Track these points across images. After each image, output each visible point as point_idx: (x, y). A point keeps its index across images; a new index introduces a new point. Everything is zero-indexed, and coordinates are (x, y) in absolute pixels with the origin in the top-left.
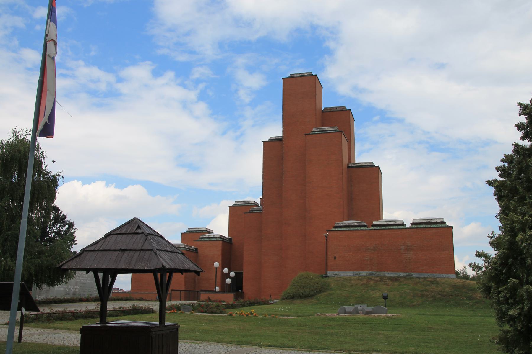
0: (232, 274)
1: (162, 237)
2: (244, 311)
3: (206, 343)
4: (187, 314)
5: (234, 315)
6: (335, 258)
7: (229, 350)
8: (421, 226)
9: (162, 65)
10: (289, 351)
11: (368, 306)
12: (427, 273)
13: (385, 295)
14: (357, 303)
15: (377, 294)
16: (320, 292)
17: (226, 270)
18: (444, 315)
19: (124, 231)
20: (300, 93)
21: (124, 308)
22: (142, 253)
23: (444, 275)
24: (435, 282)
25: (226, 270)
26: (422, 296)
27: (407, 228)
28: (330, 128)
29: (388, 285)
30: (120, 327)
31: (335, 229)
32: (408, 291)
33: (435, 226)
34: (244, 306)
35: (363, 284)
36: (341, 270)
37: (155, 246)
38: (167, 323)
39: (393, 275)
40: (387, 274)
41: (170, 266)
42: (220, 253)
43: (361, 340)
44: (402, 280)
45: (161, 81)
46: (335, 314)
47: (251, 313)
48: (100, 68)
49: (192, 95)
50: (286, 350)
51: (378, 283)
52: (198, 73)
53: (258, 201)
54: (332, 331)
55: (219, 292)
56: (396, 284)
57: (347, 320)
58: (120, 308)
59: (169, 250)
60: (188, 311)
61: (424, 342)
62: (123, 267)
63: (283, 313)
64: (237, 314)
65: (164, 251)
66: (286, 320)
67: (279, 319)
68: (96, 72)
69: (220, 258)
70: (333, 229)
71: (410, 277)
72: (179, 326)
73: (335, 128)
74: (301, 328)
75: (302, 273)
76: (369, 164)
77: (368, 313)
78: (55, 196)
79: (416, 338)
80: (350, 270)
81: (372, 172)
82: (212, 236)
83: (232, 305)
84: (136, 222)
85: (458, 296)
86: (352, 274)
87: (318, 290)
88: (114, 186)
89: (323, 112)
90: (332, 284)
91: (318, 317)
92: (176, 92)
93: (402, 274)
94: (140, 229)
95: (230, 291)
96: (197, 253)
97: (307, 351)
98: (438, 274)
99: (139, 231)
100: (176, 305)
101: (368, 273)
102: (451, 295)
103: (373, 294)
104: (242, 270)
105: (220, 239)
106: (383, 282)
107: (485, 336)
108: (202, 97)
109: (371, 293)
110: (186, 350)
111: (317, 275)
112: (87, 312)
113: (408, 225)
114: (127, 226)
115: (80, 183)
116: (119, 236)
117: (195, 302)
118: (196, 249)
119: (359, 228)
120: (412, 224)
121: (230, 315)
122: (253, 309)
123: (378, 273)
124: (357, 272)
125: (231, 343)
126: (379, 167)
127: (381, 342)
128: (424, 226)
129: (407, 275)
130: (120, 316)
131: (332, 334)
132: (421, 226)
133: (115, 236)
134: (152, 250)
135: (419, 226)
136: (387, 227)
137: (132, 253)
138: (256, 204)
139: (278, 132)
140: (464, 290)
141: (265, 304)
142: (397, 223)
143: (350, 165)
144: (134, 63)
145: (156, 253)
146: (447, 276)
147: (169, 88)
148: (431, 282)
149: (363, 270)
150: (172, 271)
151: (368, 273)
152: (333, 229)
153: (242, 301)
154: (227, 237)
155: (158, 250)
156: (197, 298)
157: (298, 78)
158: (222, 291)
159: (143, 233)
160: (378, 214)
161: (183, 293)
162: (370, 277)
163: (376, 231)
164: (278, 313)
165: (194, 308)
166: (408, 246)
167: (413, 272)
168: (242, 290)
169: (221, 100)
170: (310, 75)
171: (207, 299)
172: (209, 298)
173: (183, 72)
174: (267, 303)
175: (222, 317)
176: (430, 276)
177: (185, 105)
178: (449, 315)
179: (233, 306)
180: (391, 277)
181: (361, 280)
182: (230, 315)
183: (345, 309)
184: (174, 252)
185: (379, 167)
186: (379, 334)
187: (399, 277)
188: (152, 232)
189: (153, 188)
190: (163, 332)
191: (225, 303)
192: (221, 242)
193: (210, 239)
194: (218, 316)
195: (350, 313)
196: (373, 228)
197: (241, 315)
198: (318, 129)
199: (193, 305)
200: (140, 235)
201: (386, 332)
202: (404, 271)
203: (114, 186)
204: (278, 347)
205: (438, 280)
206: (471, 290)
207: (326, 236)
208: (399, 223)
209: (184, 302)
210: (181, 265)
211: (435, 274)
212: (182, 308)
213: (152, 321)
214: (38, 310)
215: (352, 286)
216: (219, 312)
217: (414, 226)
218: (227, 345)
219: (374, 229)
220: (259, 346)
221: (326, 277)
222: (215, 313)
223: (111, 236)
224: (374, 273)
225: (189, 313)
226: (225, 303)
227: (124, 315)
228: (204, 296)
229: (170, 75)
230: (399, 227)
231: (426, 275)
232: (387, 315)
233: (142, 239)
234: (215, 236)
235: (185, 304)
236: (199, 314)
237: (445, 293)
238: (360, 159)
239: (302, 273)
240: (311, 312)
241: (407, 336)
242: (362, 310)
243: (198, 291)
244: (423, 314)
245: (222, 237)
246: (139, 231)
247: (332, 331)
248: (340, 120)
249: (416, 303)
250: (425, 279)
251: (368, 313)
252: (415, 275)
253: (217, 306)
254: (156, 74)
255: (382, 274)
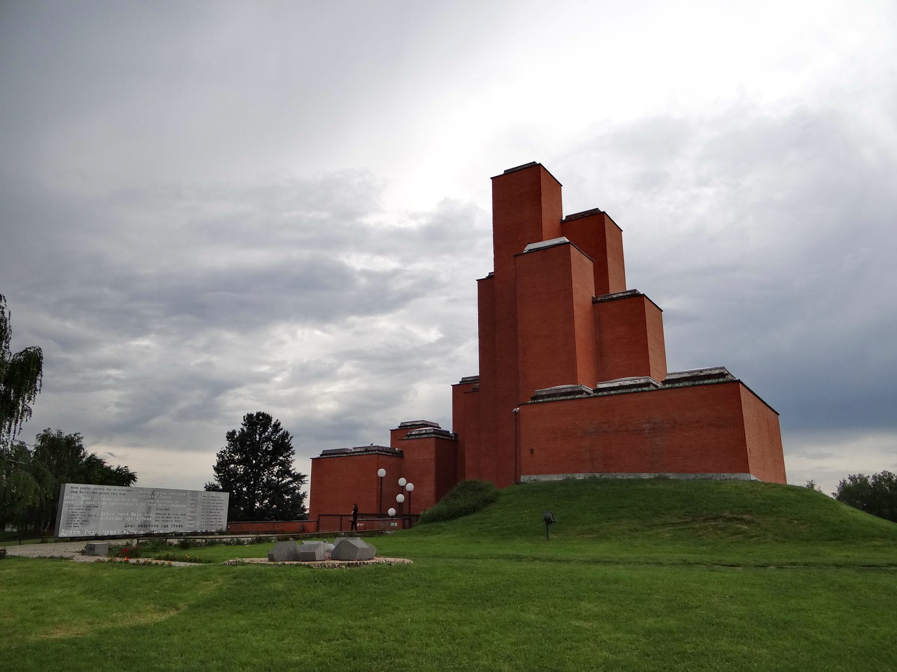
6: (532, 451)
42: (433, 456)
78: (508, 173)
80: (557, 472)
96: (402, 457)
98: (715, 474)
118: (401, 452)
124: (569, 475)
166: (655, 423)
192: (433, 440)
202: (649, 471)
214: (304, 495)
219: (718, 383)
224: (597, 475)
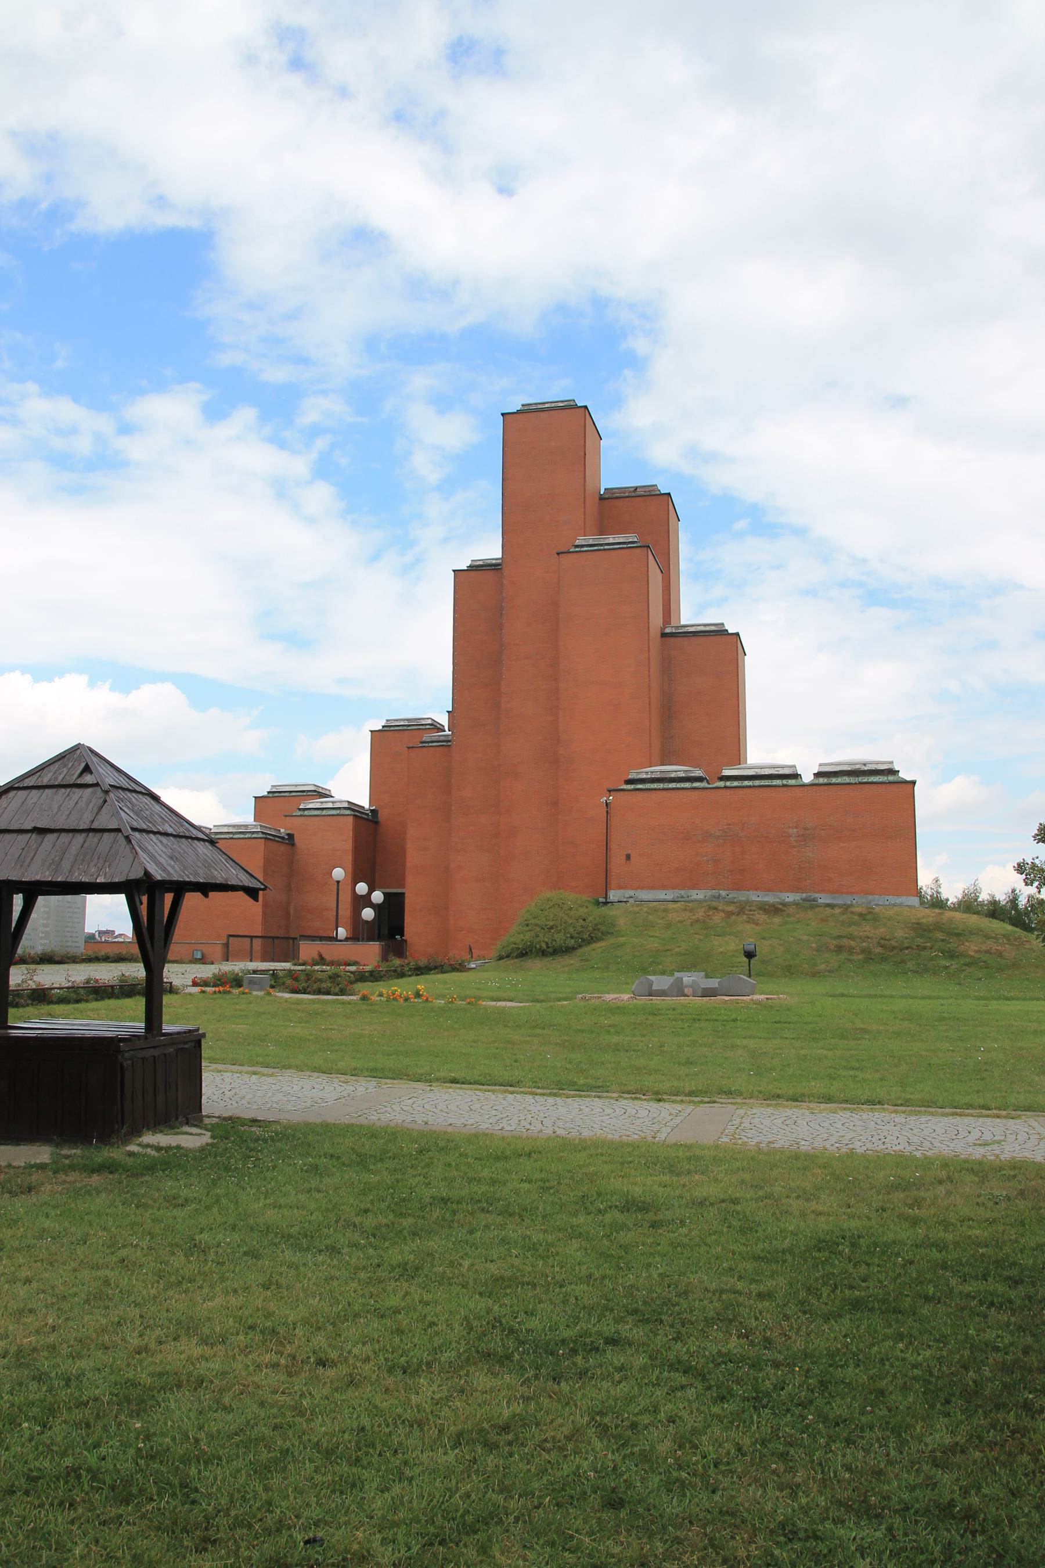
0: (377, 897)
1: (156, 798)
2: (401, 987)
3: (288, 1072)
4: (257, 997)
5: (375, 998)
6: (628, 857)
7: (345, 1093)
8: (839, 780)
9: (226, 392)
10: (500, 1096)
11: (707, 976)
12: (851, 893)
13: (751, 948)
14: (682, 969)
15: (731, 946)
16: (592, 940)
17: (362, 888)
18: (892, 997)
19: (46, 780)
20: (546, 449)
21: (97, 981)
22: (93, 838)
23: (892, 899)
24: (869, 916)
25: (362, 888)
26: (840, 949)
27: (804, 785)
28: (620, 538)
29: (757, 924)
30: (36, 1039)
31: (629, 787)
32: (806, 938)
33: (872, 779)
34: (402, 975)
35: (697, 921)
36: (642, 888)
37: (128, 819)
38: (167, 1028)
39: (770, 898)
40: (755, 896)
41: (169, 874)
43: (689, 1063)
44: (791, 910)
45: (225, 430)
46: (625, 997)
47: (418, 995)
48: (76, 400)
49: (299, 466)
50: (493, 1091)
51: (734, 917)
52: (313, 411)
53: (444, 720)
54: (616, 1039)
55: (347, 939)
56: (777, 920)
57: (654, 1012)
58: (88, 981)
59: (170, 831)
60: (261, 989)
61: (845, 1067)
62: (38, 878)
63: (495, 994)
64: (381, 995)
65: (155, 833)
66: (502, 1011)
67: (486, 1008)
68: (67, 410)
69: (349, 858)
70: (625, 787)
71: (810, 904)
72: (204, 1035)
73: (632, 537)
74: (539, 1031)
75: (548, 894)
76: (713, 628)
77: (708, 993)
79: (826, 1057)
80: (665, 887)
81: (722, 647)
82: (330, 805)
83: (371, 972)
84: (81, 756)
85: (924, 948)
86: (670, 897)
87: (585, 936)
88: (108, 685)
89: (602, 498)
90: (621, 922)
91: (583, 1003)
92: (261, 459)
93: (790, 897)
94: (91, 773)
95: (370, 939)
96: (293, 845)
97: (550, 1094)
98: (877, 897)
99: (88, 779)
100: (232, 972)
101: (710, 893)
102: (907, 948)
103: (720, 946)
104: (403, 886)
105: (348, 812)
106: (745, 917)
107: (995, 1049)
108: (323, 470)
109: (716, 943)
110: (232, 1093)
111: (584, 898)
112: (73, 989)
113: (807, 778)
114: (57, 765)
115: (28, 677)
116: (34, 792)
117: (287, 965)
118: (291, 836)
119: (687, 785)
120: (818, 775)
121: (364, 998)
122: (421, 984)
123: (733, 895)
124: (682, 892)
125: (355, 1073)
126: (737, 634)
127: (740, 1070)
128: (847, 779)
129: (804, 900)
130: (87, 1001)
131: (616, 1049)
132: (839, 780)
133: (22, 794)
134: (118, 830)
135: (834, 780)
136: (757, 783)
137: (64, 838)
138: (436, 727)
139: (492, 550)
140: (939, 935)
141: (454, 969)
142: (781, 772)
143: (668, 630)
144: (160, 386)
145: (128, 839)
146: (898, 900)
147: (243, 449)
148: (861, 915)
149: (695, 886)
150: (180, 889)
151: (710, 893)
152: (625, 787)
153: (397, 962)
154: (367, 805)
155: (134, 829)
156: (289, 955)
157: (541, 414)
158: (353, 938)
159: (97, 785)
160: (736, 750)
161: (257, 943)
162: (714, 904)
163: (728, 791)
164: (485, 994)
165: (276, 980)
166: (806, 829)
167: (819, 892)
168: (402, 935)
169: (366, 478)
170: (570, 407)
171: (317, 957)
172: (320, 955)
173: (277, 409)
174: (460, 968)
175: (344, 1003)
176: (858, 902)
177: (281, 490)
178: (903, 997)
179: (374, 976)
180: (765, 903)
181: (691, 911)
182: (364, 998)
183: (651, 984)
184: (187, 838)
185: (737, 634)
186: (734, 1047)
187: (784, 904)
188: (124, 783)
189: (200, 691)
190: (156, 1053)
191: (353, 968)
193: (324, 813)
194: (334, 1001)
195: (662, 993)
196: (721, 784)
197: (393, 998)
198: (590, 539)
199: (274, 974)
200: (90, 790)
201: (751, 1043)
203: (108, 685)
204: (475, 1083)
205: (877, 909)
206: (958, 935)
207: (607, 804)
208: (787, 771)
209: (253, 965)
210: (201, 871)
211: (870, 897)
212: (245, 982)
213: (124, 1020)
215: (669, 925)
216: (337, 990)
217: (821, 780)
218: (343, 1078)
220: (426, 1081)
221: (606, 903)
222: (328, 993)
223: (12, 793)
224: (723, 893)
225: (261, 993)
226: (353, 968)
227: (96, 1000)
228: (307, 950)
229: (246, 415)
230: (785, 782)
231: (848, 899)
232: (756, 997)
233: (94, 801)
234: (337, 805)
235: (255, 972)
236: (287, 995)
237: (893, 943)
238: (693, 610)
239: (548, 894)
240: (568, 990)
241: (803, 1052)
242: (693, 985)
243: (294, 939)
244: (842, 995)
245: (352, 807)
246: (88, 779)
247: (616, 1039)
248: (643, 520)
249: (823, 966)
250: (846, 908)
251: (708, 993)
252: (823, 899)
253: (334, 977)
254: (214, 413)
255: (742, 896)
